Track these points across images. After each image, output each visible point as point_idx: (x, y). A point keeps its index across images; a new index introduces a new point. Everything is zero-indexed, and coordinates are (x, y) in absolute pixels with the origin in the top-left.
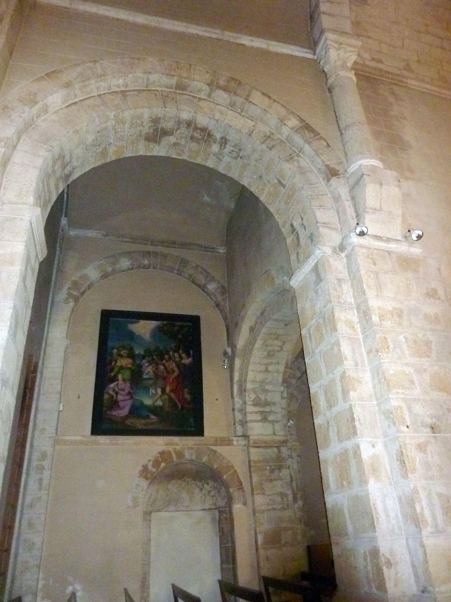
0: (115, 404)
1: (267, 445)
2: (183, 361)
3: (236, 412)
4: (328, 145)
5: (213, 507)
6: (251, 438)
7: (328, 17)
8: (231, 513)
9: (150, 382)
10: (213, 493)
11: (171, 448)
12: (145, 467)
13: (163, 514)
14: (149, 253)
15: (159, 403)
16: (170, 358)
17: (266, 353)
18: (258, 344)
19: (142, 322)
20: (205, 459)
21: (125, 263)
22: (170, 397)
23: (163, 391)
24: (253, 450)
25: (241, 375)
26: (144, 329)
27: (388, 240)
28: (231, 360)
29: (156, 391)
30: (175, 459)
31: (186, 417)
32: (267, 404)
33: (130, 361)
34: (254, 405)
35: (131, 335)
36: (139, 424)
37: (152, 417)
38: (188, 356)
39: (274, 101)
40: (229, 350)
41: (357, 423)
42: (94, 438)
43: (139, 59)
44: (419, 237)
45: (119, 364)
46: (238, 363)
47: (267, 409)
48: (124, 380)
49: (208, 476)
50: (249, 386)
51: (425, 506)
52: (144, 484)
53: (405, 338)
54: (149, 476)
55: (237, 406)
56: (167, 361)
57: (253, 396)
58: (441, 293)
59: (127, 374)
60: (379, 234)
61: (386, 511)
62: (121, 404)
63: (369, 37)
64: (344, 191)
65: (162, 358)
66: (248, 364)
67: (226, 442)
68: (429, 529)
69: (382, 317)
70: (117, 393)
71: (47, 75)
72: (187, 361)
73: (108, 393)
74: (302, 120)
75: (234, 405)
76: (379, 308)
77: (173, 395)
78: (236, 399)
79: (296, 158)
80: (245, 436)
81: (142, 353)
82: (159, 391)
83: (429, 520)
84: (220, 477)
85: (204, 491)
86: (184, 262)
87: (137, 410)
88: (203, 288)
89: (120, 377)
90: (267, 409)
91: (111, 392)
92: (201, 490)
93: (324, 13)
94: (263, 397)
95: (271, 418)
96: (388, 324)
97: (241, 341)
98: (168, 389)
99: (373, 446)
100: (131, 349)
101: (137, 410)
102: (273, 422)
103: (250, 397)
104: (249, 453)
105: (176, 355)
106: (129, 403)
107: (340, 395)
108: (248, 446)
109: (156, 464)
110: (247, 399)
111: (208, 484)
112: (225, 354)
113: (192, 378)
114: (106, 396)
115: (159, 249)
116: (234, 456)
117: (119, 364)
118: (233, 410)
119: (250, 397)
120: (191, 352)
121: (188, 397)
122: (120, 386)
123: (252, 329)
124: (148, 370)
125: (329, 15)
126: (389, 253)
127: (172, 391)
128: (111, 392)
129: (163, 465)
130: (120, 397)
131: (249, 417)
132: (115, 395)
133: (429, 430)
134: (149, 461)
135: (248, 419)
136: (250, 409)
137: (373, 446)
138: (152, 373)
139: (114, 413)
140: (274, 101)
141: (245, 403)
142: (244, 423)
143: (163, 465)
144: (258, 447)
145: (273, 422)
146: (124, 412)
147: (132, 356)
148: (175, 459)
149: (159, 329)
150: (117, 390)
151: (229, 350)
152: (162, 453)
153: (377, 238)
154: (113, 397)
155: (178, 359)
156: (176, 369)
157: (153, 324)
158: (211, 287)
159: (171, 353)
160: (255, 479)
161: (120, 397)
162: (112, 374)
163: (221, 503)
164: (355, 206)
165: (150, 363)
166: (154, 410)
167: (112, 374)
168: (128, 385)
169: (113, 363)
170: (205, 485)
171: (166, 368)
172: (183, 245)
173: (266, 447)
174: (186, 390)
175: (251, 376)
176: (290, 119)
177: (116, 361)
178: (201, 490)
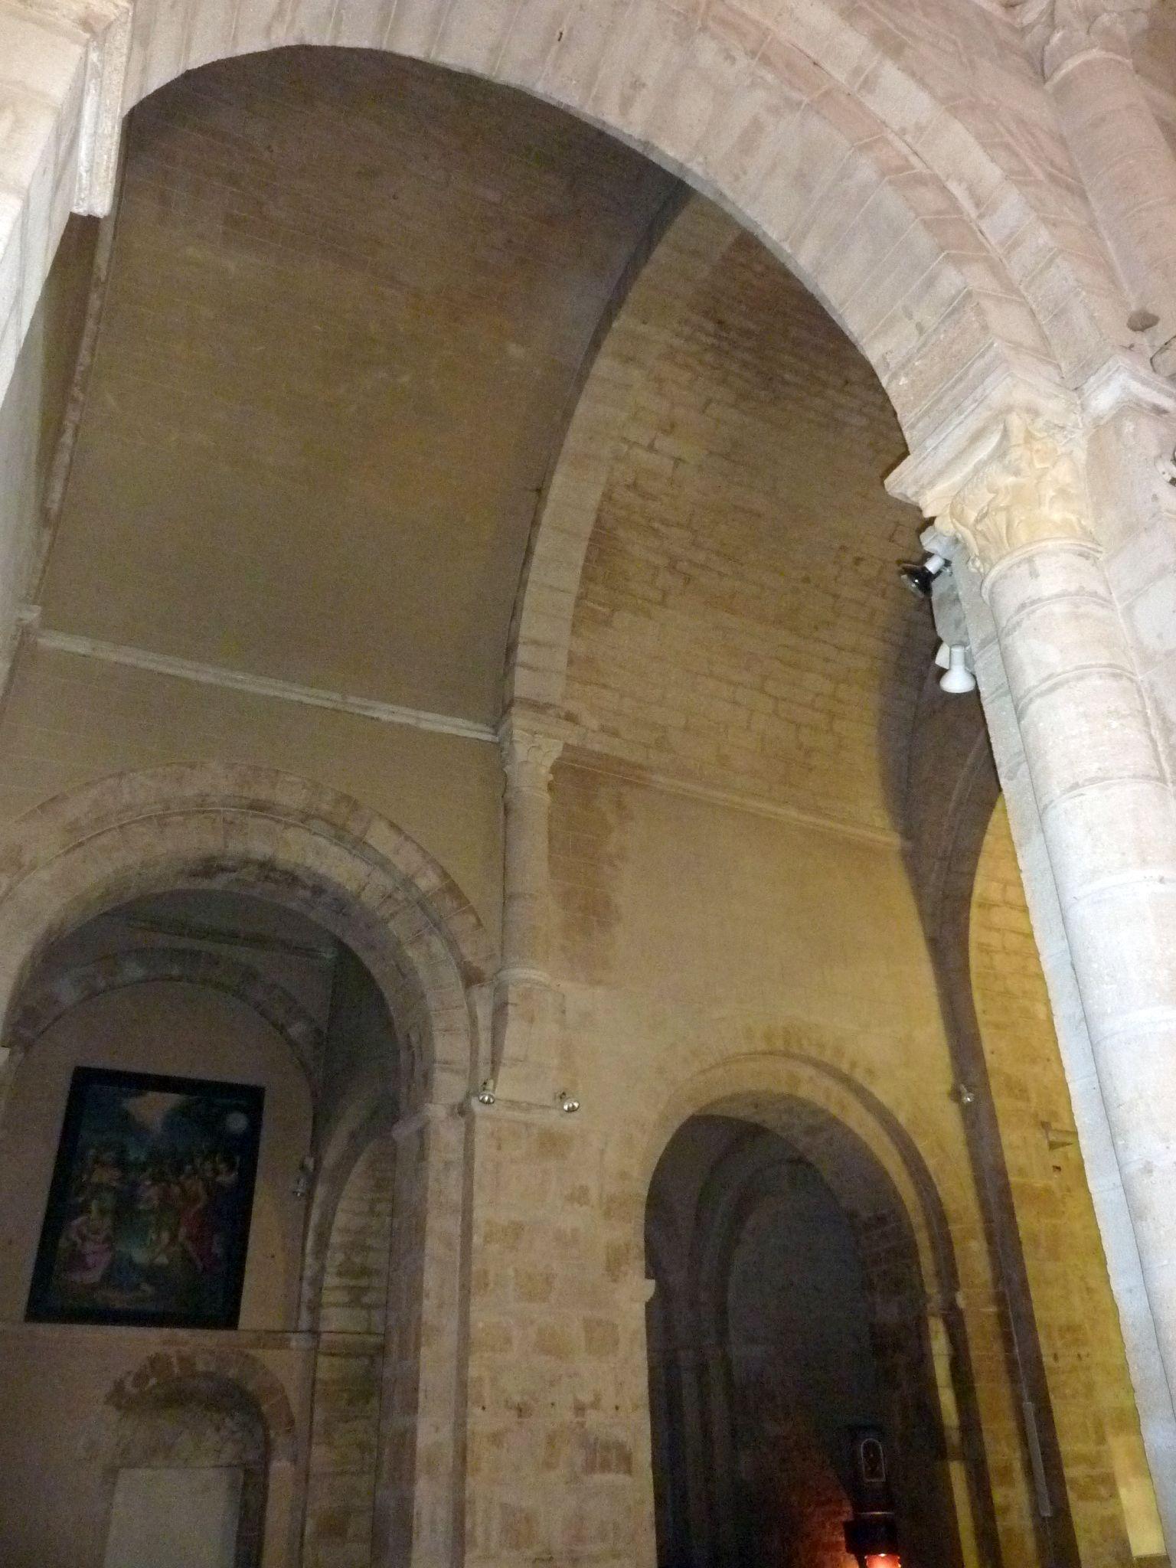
0: (77, 1260)
1: (349, 1353)
2: (219, 1179)
3: (305, 1285)
4: (479, 924)
5: (235, 1462)
6: (324, 1337)
7: (526, 672)
8: (266, 1473)
9: (152, 1218)
10: (239, 1435)
11: (172, 1351)
12: (119, 1387)
13: (141, 1473)
14: (183, 952)
15: (162, 1260)
16: (195, 1172)
17: (372, 1182)
18: (360, 1166)
19: (152, 1095)
20: (232, 1373)
21: (134, 971)
22: (185, 1251)
23: (173, 1239)
24: (323, 1362)
25: (323, 1215)
26: (153, 1110)
27: (529, 1107)
28: (312, 1181)
29: (159, 1236)
30: (176, 1370)
31: (209, 1295)
32: (364, 1272)
33: (117, 1173)
34: (340, 1274)
35: (127, 1123)
36: (119, 1300)
37: (145, 1287)
38: (231, 1167)
39: (407, 838)
40: (310, 1163)
41: (421, 1396)
42: (31, 1327)
43: (192, 767)
44: (572, 1110)
45: (95, 1179)
46: (320, 1192)
47: (363, 1282)
48: (102, 1212)
49: (237, 1402)
50: (336, 1239)
51: (479, 1521)
52: (113, 1415)
53: (516, 1270)
54: (123, 1402)
55: (308, 1273)
56: (188, 1177)
57: (340, 1257)
58: (594, 1194)
59: (109, 1200)
60: (516, 1098)
61: (433, 1522)
62: (90, 1260)
63: (605, 686)
64: (484, 1013)
65: (179, 1170)
66: (338, 1197)
67: (276, 1339)
68: (478, 1552)
69: (488, 1239)
70: (84, 1238)
71: (42, 807)
72: (227, 1178)
73: (68, 1239)
74: (445, 875)
75: (303, 1269)
76: (488, 1222)
77: (190, 1247)
78: (309, 1260)
79: (426, 937)
80: (314, 1332)
81: (143, 1158)
82: (165, 1236)
83: (480, 1540)
84: (258, 1406)
85: (224, 1433)
86: (250, 975)
87: (118, 1272)
88: (282, 1029)
89: (94, 1206)
90: (363, 1282)
91: (73, 1236)
92: (218, 1429)
93: (524, 665)
94: (358, 1260)
95: (366, 1300)
96: (494, 1248)
97: (331, 1156)
98: (183, 1232)
99: (437, 1430)
100: (123, 1151)
101: (118, 1272)
102: (368, 1307)
103: (335, 1258)
104: (314, 1367)
105: (208, 1165)
106: (106, 1258)
107: (412, 1348)
108: (316, 1350)
109: (140, 1378)
110: (328, 1263)
111: (232, 1416)
112: (303, 1167)
113: (232, 1215)
114: (63, 1243)
115: (206, 946)
116: (284, 1367)
117: (95, 1179)
118: (301, 1279)
119: (335, 1258)
120: (238, 1159)
121: (218, 1250)
122: (89, 1229)
123: (353, 1135)
124: (150, 1194)
125: (530, 668)
126: (527, 1125)
127: (189, 1238)
128: (73, 1236)
129: (153, 1381)
130: (89, 1247)
131: (328, 1297)
132: (79, 1241)
133: (514, 1412)
134: (129, 1373)
135: (324, 1299)
136: (330, 1280)
137: (437, 1430)
138: (156, 1202)
139: (76, 1277)
140: (407, 838)
141: (323, 1268)
142: (315, 1307)
143: (153, 1381)
144: (333, 1355)
145: (368, 1307)
146: (93, 1276)
147: (121, 1164)
148: (176, 1370)
149: (183, 1111)
150: (85, 1231)
151: (310, 1163)
152: (153, 1361)
153: (513, 1104)
154: (75, 1244)
155: (209, 1174)
156: (204, 1197)
157: (171, 1100)
158: (297, 1029)
159: (198, 1161)
160: (319, 1416)
161: (89, 1247)
162: (80, 1199)
163: (251, 1456)
164: (493, 1043)
165: (155, 1180)
166: (152, 1273)
167: (80, 1199)
168: (108, 1221)
169: (85, 1177)
170: (227, 1420)
171: (184, 1190)
172: (258, 941)
173: (348, 1355)
174: (216, 1238)
175: (341, 1219)
176: (425, 875)
177: (91, 1173)
178: (218, 1429)
